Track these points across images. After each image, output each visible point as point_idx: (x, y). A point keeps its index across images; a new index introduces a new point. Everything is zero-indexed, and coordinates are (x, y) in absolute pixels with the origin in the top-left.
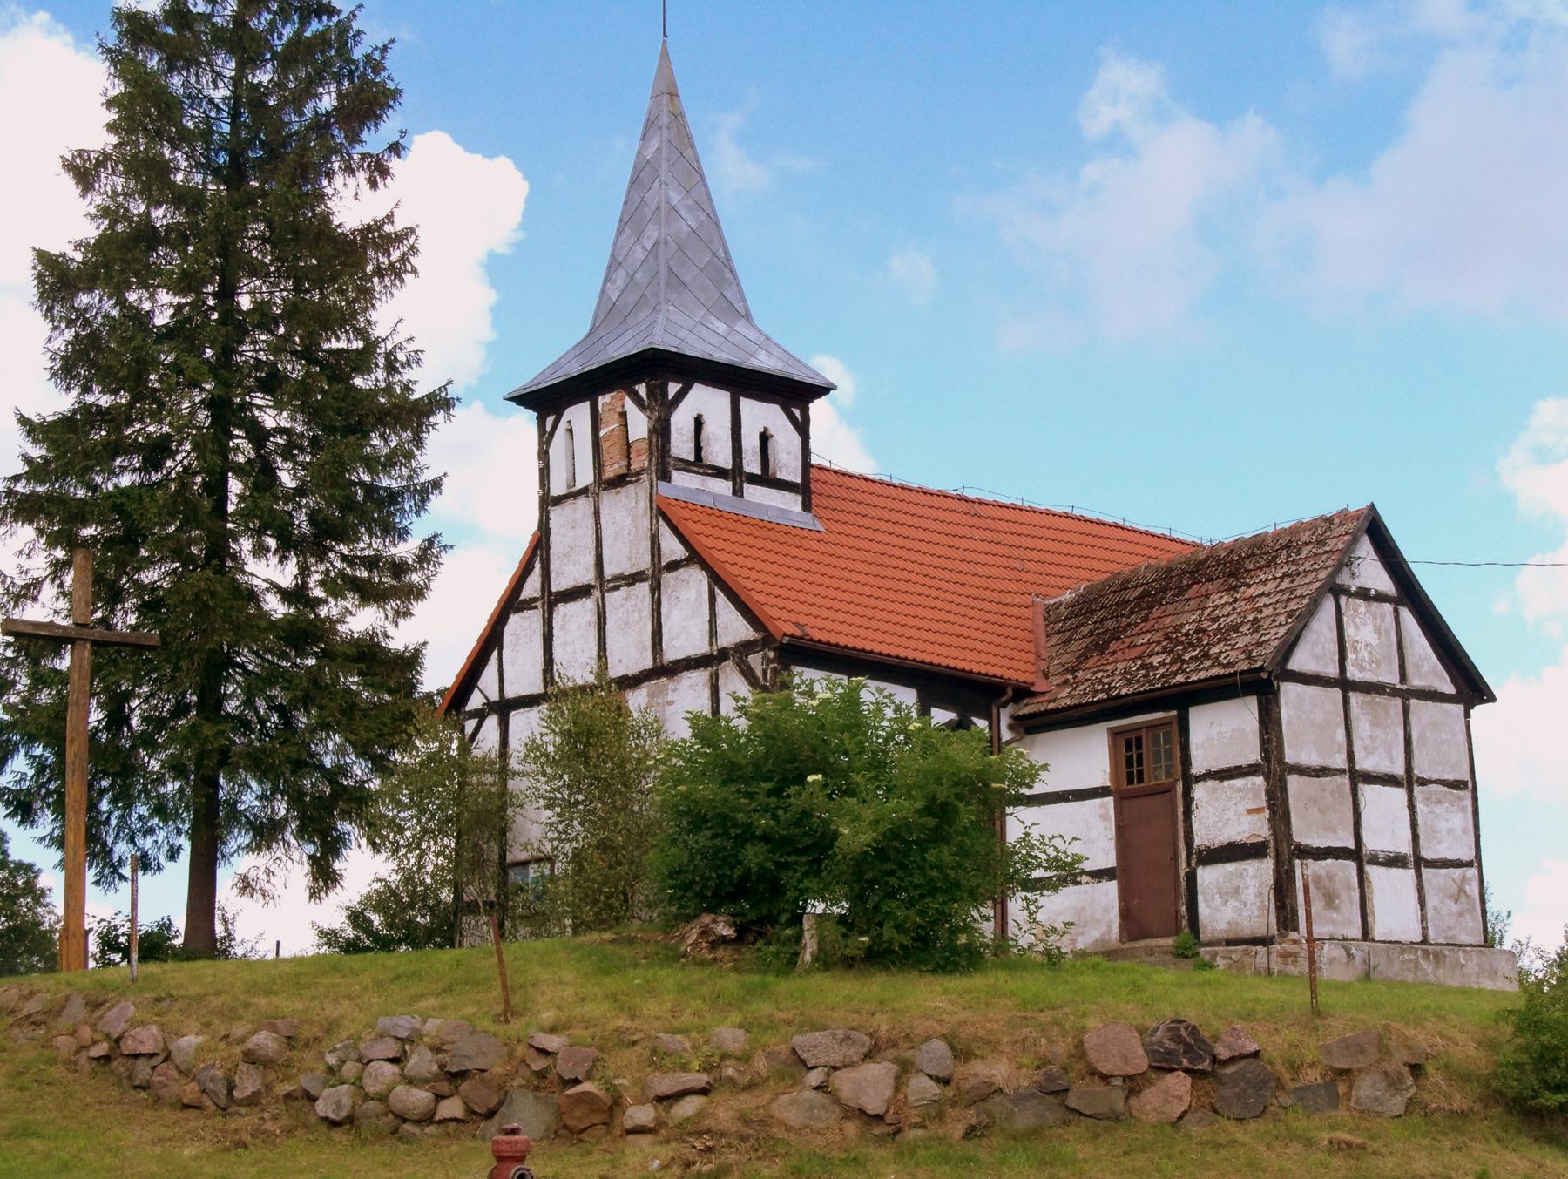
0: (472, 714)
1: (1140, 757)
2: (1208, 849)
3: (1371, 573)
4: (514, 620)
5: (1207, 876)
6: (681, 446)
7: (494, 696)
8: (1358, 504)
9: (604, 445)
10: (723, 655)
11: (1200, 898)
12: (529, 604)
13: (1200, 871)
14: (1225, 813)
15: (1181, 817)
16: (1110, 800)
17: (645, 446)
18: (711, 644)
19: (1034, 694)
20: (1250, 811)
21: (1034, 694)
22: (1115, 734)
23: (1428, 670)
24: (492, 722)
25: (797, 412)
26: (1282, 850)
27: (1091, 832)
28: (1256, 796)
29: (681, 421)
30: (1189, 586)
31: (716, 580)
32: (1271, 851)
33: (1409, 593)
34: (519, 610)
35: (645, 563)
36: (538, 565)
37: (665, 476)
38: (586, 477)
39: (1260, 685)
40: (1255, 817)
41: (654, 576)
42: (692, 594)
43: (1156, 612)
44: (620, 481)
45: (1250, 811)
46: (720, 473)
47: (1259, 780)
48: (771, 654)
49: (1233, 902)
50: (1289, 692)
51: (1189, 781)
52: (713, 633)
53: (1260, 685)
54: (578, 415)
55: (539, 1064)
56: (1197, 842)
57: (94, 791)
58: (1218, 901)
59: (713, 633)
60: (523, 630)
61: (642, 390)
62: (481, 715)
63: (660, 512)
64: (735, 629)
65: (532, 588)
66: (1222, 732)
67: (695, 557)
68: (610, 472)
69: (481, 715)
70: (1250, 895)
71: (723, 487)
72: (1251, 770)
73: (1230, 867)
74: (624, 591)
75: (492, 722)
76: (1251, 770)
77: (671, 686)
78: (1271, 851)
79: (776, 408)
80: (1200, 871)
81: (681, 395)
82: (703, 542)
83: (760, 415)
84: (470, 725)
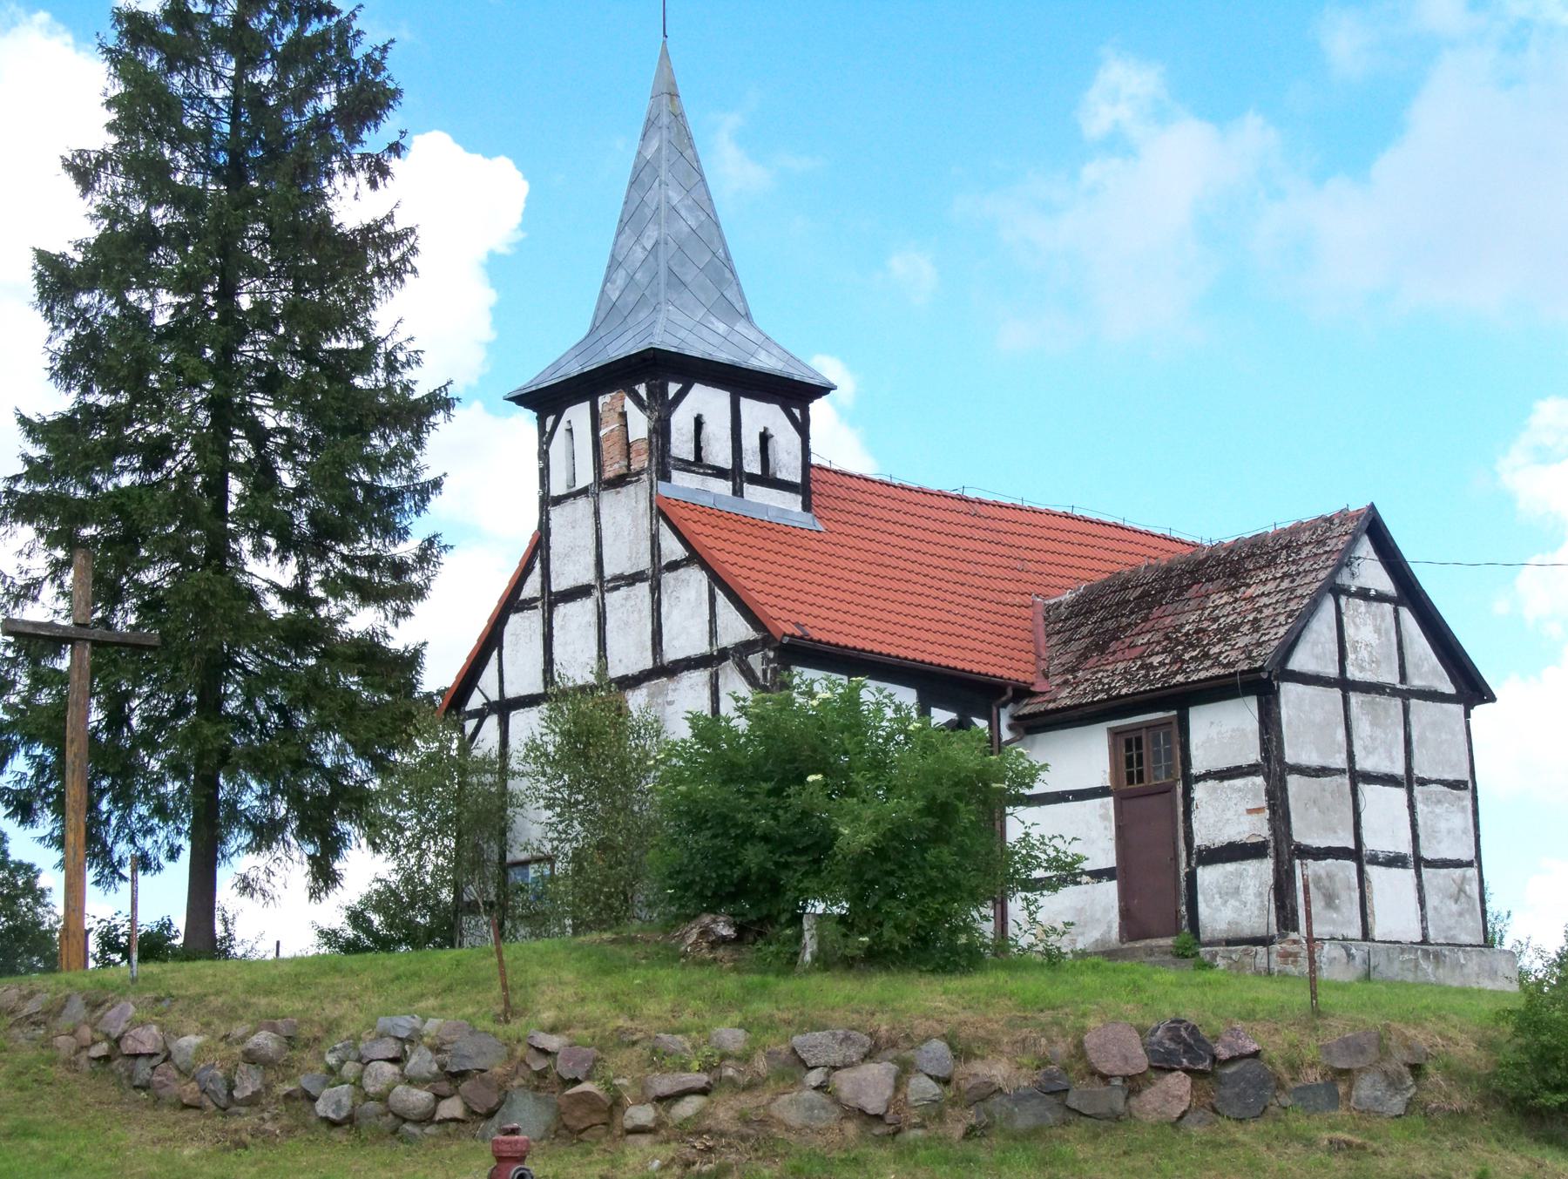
0: (472, 714)
1: (1140, 757)
2: (1208, 849)
3: (1371, 573)
4: (514, 620)
5: (1207, 876)
6: (681, 446)
7: (494, 696)
8: (1358, 504)
9: (604, 445)
10: (723, 655)
11: (1200, 898)
12: (529, 604)
13: (1200, 871)
14: (1225, 813)
15: (1181, 817)
17: (645, 446)
18: (711, 644)
19: (1034, 694)
20: (1250, 811)
21: (1034, 694)
22: (1114, 734)
23: (1428, 670)
24: (492, 722)
25: (797, 412)
26: (1282, 850)
27: (1091, 832)
28: (1256, 796)
29: (681, 422)
30: (1189, 586)
32: (1271, 851)
33: (1409, 593)
34: (519, 610)
35: (644, 563)
36: (538, 565)
37: (666, 477)
38: (586, 477)
40: (1255, 817)
41: (654, 576)
42: (692, 594)
44: (620, 481)
45: (1250, 811)
47: (1259, 780)
48: (771, 654)
49: (1233, 902)
50: (1290, 692)
52: (713, 633)
53: (1260, 685)
54: (578, 415)
56: (1197, 842)
57: (93, 791)
58: (1218, 901)
59: (713, 633)
60: (523, 630)
61: (642, 390)
62: (481, 715)
63: (660, 512)
64: (735, 629)
65: (532, 588)
66: (1222, 732)
67: (695, 557)
68: (610, 472)
69: (481, 715)
70: (1250, 894)
71: (723, 487)
72: (1251, 770)
73: (1230, 867)
74: (624, 591)
75: (492, 722)
76: (1251, 770)
77: (671, 686)
78: (1271, 851)
79: (776, 408)
80: (1200, 871)
81: (681, 395)
82: (704, 542)
83: (760, 415)
84: (470, 725)
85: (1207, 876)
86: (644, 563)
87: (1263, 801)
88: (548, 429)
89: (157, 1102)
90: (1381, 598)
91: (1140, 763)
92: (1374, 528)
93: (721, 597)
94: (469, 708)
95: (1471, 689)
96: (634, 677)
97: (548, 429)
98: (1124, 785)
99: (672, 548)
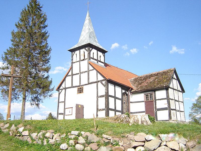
0: (61, 89)
1: (146, 98)
3: (175, 77)
4: (67, 78)
5: (158, 112)
6: (92, 56)
7: (64, 87)
8: (172, 68)
10: (99, 81)
12: (70, 76)
14: (161, 104)
15: (154, 105)
16: (144, 103)
19: (133, 89)
21: (133, 89)
23: (180, 89)
24: (64, 90)
25: (104, 54)
26: (169, 109)
27: (142, 107)
30: (151, 77)
31: (97, 71)
33: (178, 79)
35: (87, 70)
37: (90, 59)
38: (78, 60)
39: (167, 88)
41: (88, 71)
43: (147, 80)
44: (83, 60)
46: (96, 60)
48: (106, 81)
50: (170, 89)
51: (156, 100)
52: (97, 79)
53: (167, 88)
54: (77, 52)
55: (107, 141)
57: (11, 95)
59: (97, 79)
60: (68, 79)
62: (62, 89)
63: (89, 64)
64: (100, 78)
65: (70, 74)
66: (160, 94)
68: (82, 59)
69: (62, 89)
71: (96, 62)
72: (165, 99)
75: (64, 90)
76: (165, 99)
79: (102, 53)
81: (92, 50)
83: (100, 54)
84: (60, 91)
85: (158, 112)
86: (87, 70)
87: (167, 103)
88: (73, 54)
89: (108, 139)
90: (175, 79)
91: (146, 97)
92: (175, 72)
93: (98, 73)
94: (60, 89)
95: (183, 91)
96: (59, 95)
97: (73, 54)
98: (146, 101)
99: (91, 68)
